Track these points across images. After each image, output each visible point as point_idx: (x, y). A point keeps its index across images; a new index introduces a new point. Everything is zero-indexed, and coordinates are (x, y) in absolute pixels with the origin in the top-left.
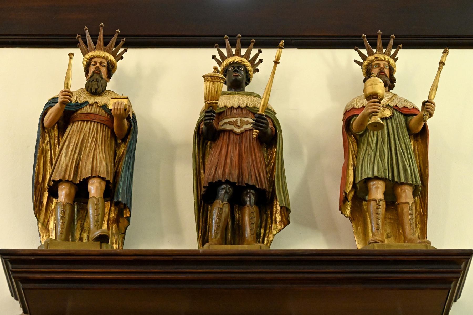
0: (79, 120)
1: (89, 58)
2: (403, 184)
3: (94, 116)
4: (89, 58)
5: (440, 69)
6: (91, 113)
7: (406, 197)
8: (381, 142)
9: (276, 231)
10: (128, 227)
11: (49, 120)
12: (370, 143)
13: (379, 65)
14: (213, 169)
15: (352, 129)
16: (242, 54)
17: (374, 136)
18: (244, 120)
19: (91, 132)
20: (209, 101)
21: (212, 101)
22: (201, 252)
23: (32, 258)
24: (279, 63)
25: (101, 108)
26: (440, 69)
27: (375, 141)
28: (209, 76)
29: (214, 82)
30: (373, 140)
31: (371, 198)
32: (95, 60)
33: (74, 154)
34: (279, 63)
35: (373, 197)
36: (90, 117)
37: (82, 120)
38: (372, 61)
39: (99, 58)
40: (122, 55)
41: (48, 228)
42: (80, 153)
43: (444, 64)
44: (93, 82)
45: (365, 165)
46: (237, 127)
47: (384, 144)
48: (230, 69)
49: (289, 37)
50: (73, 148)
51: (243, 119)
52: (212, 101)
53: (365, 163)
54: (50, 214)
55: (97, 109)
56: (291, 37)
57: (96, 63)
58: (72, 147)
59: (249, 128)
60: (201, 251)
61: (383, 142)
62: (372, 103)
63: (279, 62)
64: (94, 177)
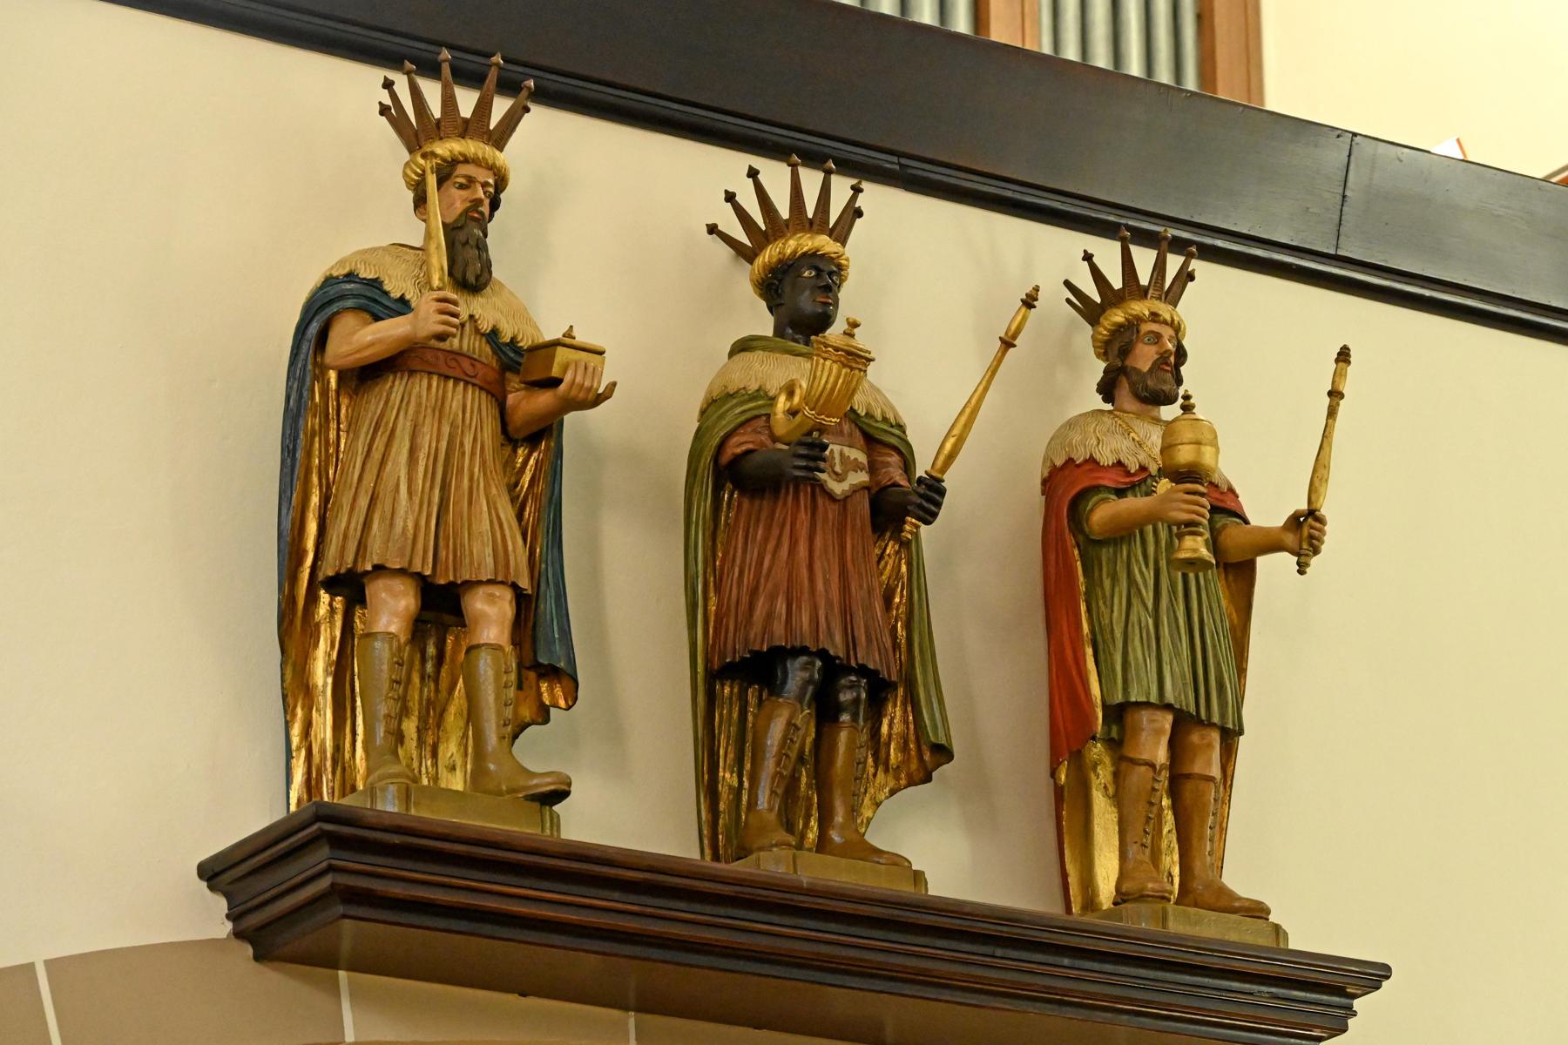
0: (432, 370)
1: (450, 160)
2: (1212, 725)
3: (473, 365)
4: (450, 160)
5: (1332, 413)
6: (459, 351)
7: (1209, 763)
8: (1169, 591)
9: (885, 793)
10: (533, 726)
11: (358, 356)
12: (1135, 581)
13: (1157, 337)
14: (782, 604)
15: (1085, 525)
16: (1116, 288)
17: (1147, 566)
18: (848, 456)
19: (468, 421)
20: (823, 417)
21: (829, 419)
22: (805, 885)
23: (397, 839)
24: (1015, 346)
25: (484, 340)
26: (1332, 413)
27: (1151, 583)
28: (842, 350)
29: (852, 369)
30: (1148, 579)
31: (1140, 754)
32: (463, 170)
33: (432, 487)
34: (1015, 346)
35: (1145, 756)
36: (460, 366)
37: (441, 372)
38: (1139, 319)
39: (480, 166)
40: (856, 206)
41: (308, 681)
42: (445, 487)
43: (1342, 396)
44: (468, 247)
45: (1136, 659)
46: (834, 477)
47: (1176, 600)
48: (806, 274)
49: (896, 155)
50: (427, 465)
51: (847, 450)
52: (829, 419)
53: (1134, 650)
54: (311, 638)
55: (475, 340)
56: (902, 157)
57: (471, 180)
58: (424, 464)
59: (860, 483)
60: (805, 881)
61: (1174, 593)
62: (1188, 493)
63: (1016, 342)
64: (502, 583)
